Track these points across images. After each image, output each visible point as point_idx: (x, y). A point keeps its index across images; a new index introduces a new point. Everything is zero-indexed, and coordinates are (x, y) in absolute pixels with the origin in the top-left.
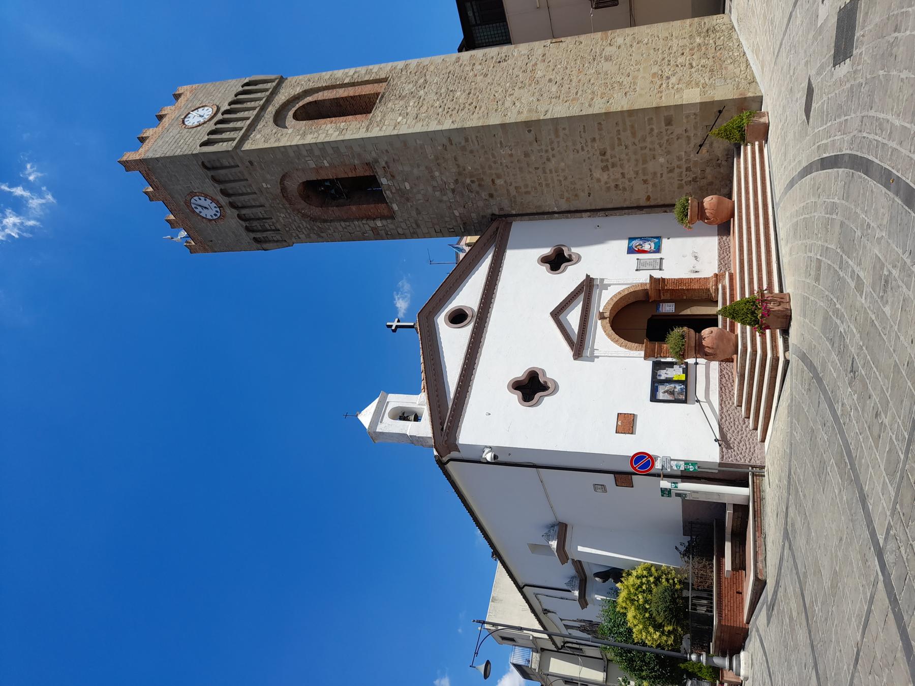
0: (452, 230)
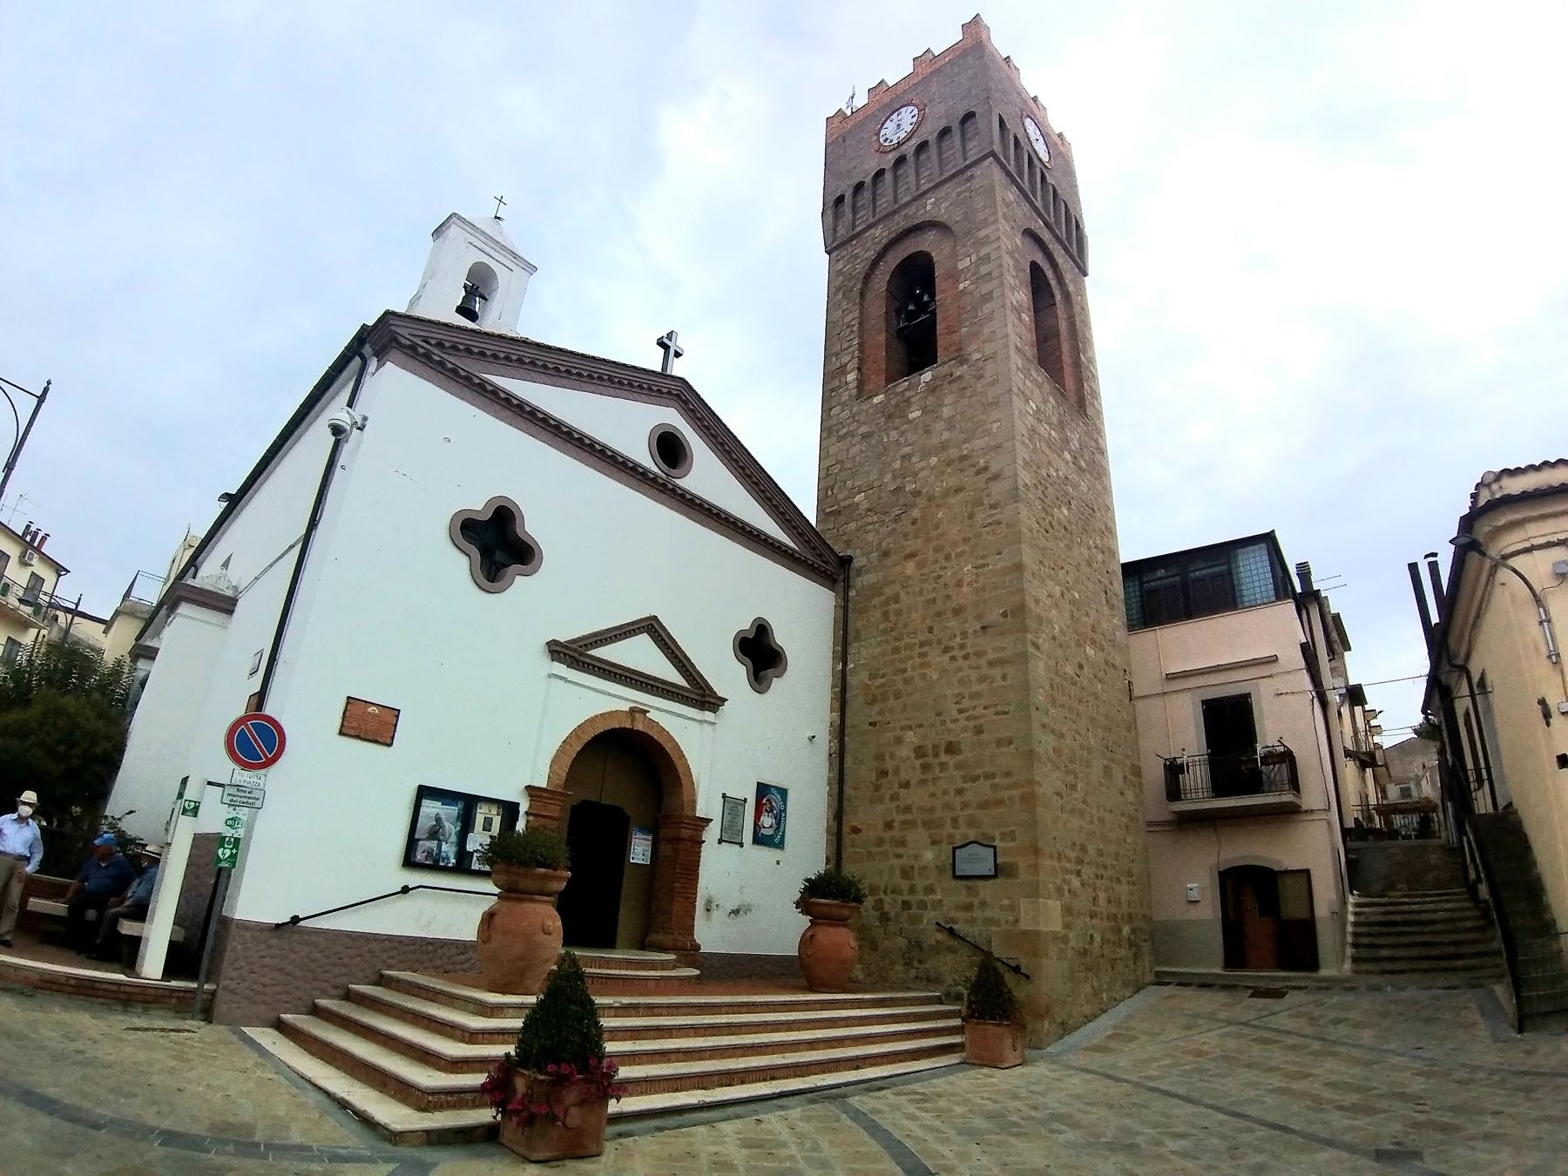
0: (830, 493)
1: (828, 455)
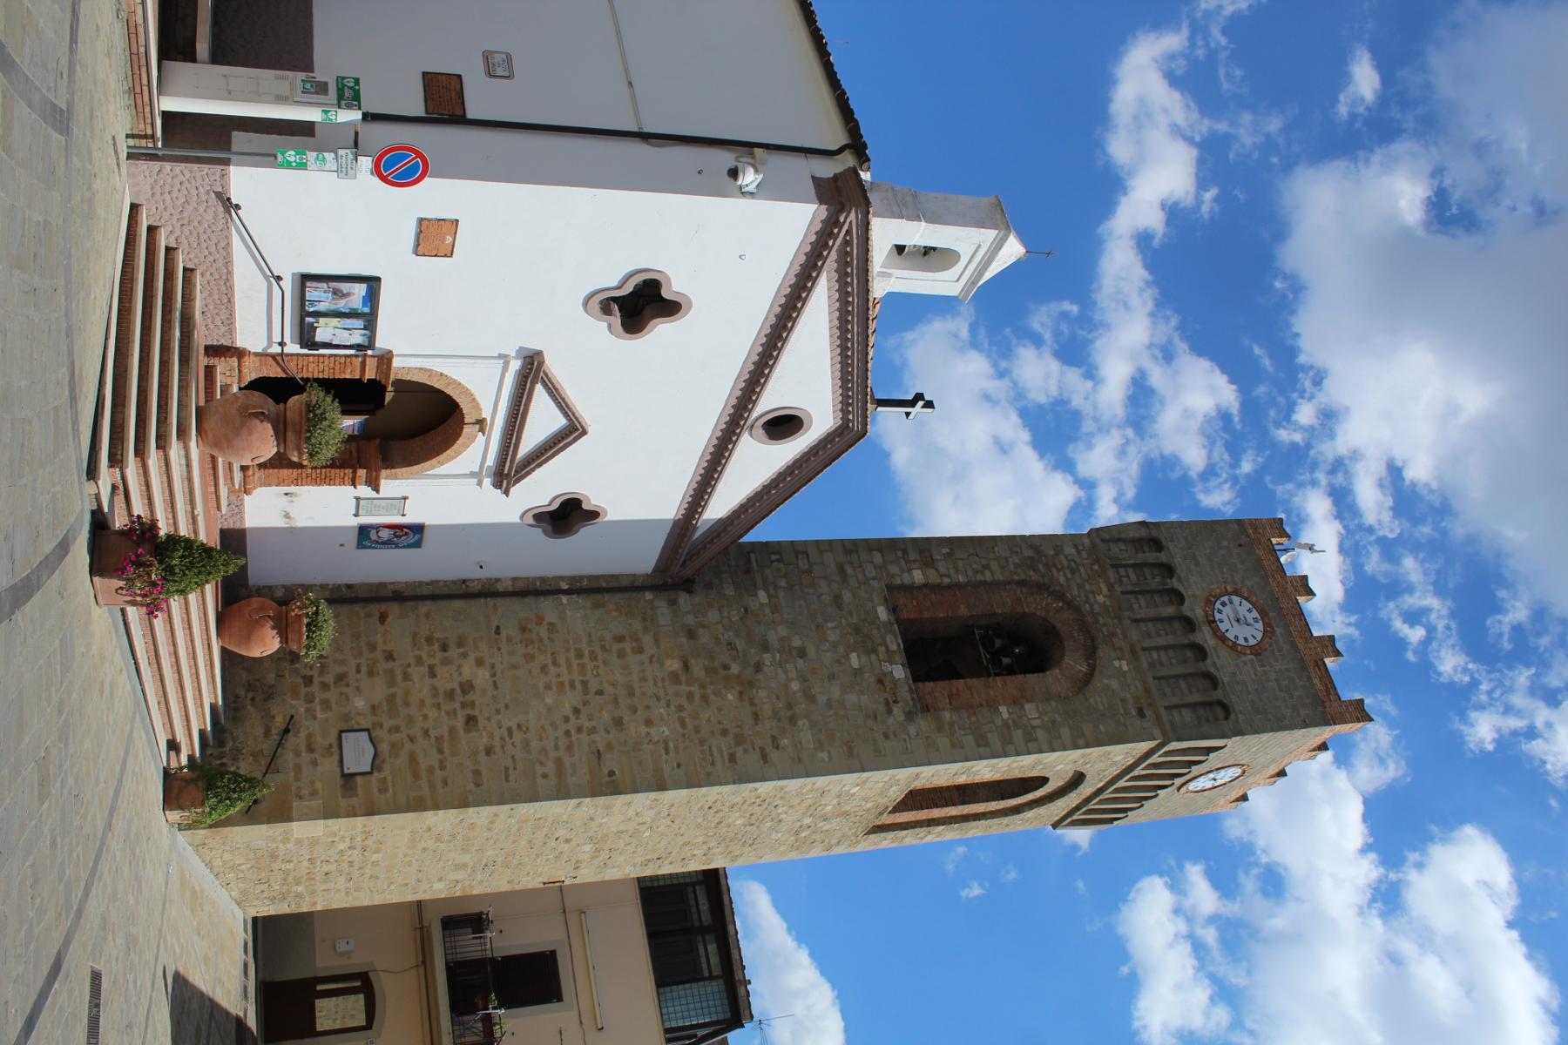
0: (774, 557)
1: (821, 552)
